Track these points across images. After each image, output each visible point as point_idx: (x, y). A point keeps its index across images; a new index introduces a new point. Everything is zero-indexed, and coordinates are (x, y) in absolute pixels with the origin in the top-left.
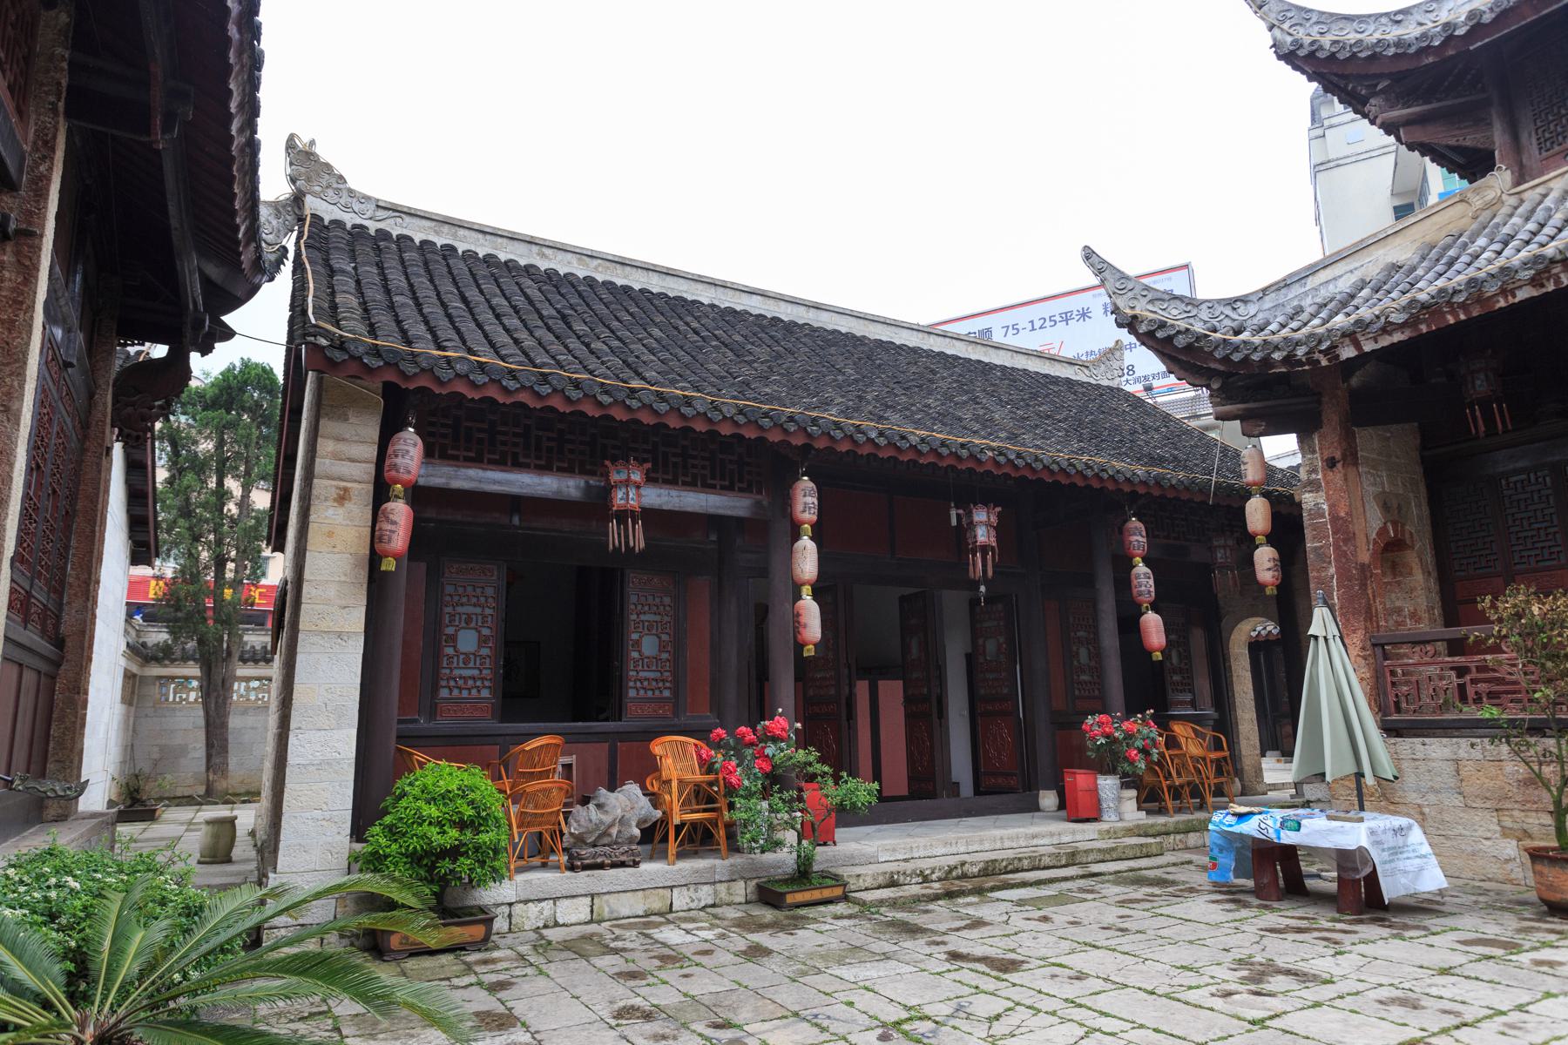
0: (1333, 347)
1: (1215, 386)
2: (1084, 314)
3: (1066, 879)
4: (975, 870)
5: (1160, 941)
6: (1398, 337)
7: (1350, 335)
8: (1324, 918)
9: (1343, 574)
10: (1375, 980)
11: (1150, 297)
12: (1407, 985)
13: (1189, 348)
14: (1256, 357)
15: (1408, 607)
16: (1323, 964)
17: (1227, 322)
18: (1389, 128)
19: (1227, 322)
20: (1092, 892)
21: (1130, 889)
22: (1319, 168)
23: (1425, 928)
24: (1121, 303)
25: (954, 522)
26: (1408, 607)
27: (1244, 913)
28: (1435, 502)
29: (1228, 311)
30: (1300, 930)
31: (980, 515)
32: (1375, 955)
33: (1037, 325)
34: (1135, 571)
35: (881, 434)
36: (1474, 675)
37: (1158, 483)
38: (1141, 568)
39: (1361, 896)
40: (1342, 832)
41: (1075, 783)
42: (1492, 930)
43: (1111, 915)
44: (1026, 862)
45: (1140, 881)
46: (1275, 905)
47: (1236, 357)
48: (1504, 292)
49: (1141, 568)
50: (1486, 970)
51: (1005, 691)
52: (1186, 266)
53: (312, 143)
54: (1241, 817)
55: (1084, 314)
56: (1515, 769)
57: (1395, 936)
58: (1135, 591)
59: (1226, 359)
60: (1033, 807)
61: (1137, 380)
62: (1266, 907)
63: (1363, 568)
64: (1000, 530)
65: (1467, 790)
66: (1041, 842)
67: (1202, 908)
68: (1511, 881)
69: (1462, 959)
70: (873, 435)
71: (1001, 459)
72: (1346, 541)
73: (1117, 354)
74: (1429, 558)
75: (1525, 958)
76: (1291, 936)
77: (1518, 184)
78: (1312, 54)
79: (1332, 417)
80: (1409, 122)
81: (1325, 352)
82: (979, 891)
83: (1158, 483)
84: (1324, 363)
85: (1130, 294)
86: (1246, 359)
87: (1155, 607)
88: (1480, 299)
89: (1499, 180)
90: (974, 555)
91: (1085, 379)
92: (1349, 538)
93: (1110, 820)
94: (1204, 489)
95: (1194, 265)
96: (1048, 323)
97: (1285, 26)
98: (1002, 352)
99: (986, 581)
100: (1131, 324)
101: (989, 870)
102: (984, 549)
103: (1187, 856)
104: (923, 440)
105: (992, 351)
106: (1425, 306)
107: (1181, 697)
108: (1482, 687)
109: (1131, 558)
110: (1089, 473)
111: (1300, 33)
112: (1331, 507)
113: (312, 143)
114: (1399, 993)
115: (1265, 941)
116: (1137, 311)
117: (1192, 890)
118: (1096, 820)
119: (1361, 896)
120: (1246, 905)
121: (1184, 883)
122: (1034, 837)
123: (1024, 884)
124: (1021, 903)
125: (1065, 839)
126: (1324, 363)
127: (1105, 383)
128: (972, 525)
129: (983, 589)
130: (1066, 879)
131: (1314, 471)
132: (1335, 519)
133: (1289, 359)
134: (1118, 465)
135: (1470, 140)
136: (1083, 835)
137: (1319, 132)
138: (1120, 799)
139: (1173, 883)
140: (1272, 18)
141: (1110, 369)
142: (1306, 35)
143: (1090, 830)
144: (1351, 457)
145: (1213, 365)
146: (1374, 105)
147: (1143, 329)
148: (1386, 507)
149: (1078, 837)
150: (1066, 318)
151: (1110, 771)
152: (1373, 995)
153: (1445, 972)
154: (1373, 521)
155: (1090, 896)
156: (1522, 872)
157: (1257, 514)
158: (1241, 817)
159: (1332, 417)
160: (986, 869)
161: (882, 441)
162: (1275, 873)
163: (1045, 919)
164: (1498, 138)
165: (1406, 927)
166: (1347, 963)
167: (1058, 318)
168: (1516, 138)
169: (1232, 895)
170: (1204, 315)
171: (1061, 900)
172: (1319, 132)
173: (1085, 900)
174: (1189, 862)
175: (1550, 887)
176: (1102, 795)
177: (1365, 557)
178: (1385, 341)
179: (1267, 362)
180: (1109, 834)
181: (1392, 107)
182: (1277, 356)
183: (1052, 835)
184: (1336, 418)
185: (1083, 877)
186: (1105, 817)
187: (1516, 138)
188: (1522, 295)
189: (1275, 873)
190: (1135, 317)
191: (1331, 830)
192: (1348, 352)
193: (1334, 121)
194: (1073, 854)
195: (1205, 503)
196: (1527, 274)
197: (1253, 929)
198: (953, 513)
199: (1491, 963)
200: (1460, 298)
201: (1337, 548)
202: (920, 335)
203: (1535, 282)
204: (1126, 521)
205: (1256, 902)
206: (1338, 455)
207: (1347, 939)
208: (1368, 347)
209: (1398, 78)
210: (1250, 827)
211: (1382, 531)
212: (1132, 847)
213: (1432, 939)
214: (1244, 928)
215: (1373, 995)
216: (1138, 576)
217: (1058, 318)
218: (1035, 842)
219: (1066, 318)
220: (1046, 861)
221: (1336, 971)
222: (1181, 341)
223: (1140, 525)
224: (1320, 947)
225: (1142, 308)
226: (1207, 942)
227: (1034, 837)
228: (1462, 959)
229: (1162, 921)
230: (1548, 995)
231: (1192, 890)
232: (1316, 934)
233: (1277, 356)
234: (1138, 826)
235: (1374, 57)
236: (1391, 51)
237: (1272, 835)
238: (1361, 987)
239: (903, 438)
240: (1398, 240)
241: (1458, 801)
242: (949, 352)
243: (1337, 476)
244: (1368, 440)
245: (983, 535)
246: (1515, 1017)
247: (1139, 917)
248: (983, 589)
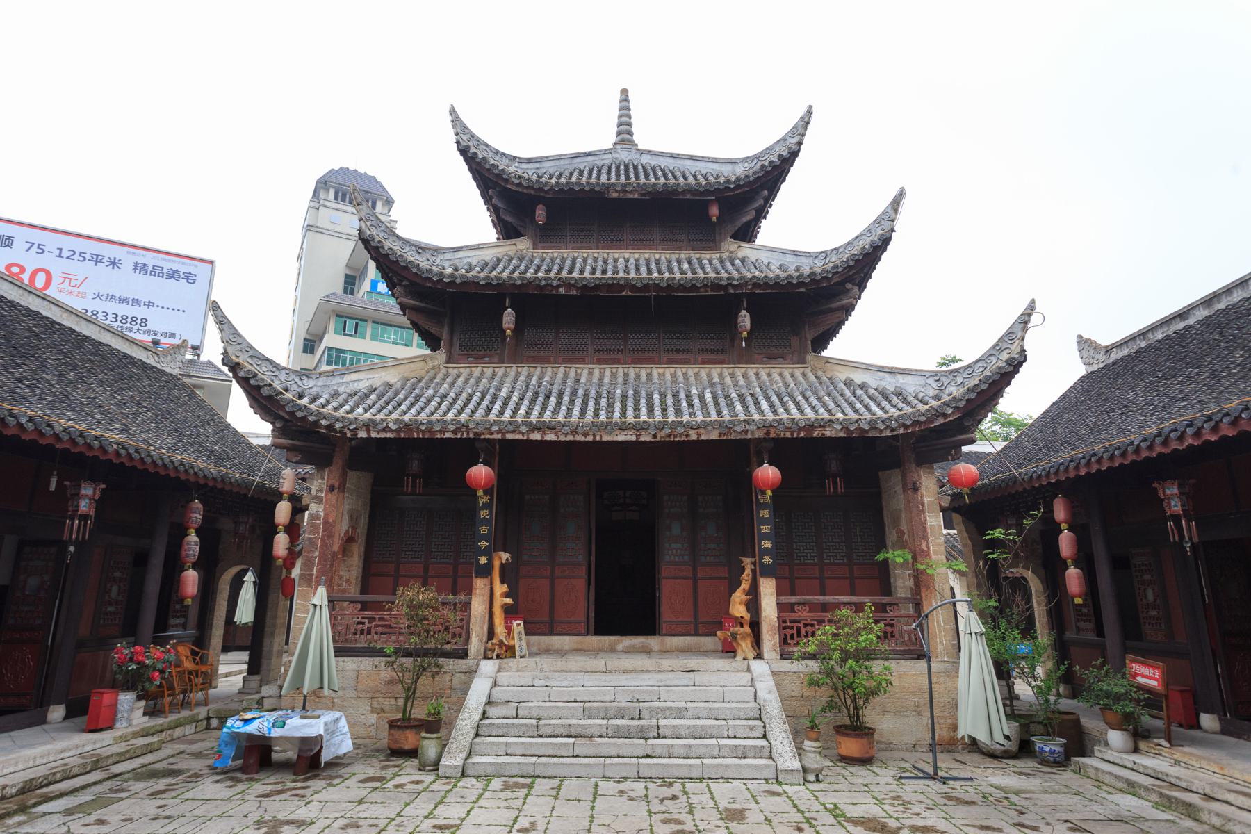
0: (356, 429)
1: (278, 425)
2: (114, 263)
3: (95, 784)
4: (14, 790)
5: (200, 820)
6: (389, 435)
7: (367, 426)
8: (288, 780)
9: (323, 556)
10: (333, 815)
11: (251, 353)
12: (348, 815)
13: (270, 398)
14: (311, 419)
15: (346, 575)
16: (302, 813)
17: (295, 387)
18: (403, 307)
19: (295, 387)
20: (122, 790)
21: (151, 783)
22: (310, 228)
23: (341, 777)
24: (230, 350)
25: (53, 487)
26: (346, 575)
27: (240, 787)
28: (372, 517)
29: (297, 380)
30: (279, 792)
31: (87, 490)
32: (324, 803)
33: (65, 253)
34: (188, 538)
35: (30, 420)
36: (377, 622)
37: (223, 480)
38: (193, 538)
39: (309, 762)
40: (310, 726)
41: (101, 701)
42: (371, 772)
43: (151, 807)
44: (58, 775)
45: (154, 775)
46: (256, 776)
47: (299, 414)
48: (441, 431)
49: (193, 538)
50: (376, 796)
51: (39, 622)
52: (211, 262)
53: (1085, 344)
54: (246, 721)
55: (114, 263)
56: (386, 674)
57: (330, 785)
58: (183, 553)
59: (292, 413)
60: (42, 720)
61: (147, 332)
62: (251, 779)
63: (334, 554)
64: (100, 504)
65: (360, 687)
66: (67, 755)
67: (210, 788)
68: (369, 737)
69: (364, 793)
70: (24, 420)
71: (123, 452)
72: (329, 537)
73: (182, 350)
74: (362, 549)
75: (390, 785)
76: (277, 798)
77: (448, 362)
78: (377, 248)
79: (338, 462)
80: (413, 308)
81: (351, 431)
82: (23, 809)
83: (223, 480)
84: (349, 435)
85: (238, 347)
86: (304, 418)
87: (195, 566)
88: (430, 430)
89: (441, 356)
90: (72, 520)
91: (154, 364)
92: (331, 536)
93: (121, 728)
94: (248, 485)
95: (217, 264)
96: (76, 257)
97: (369, 223)
98: (92, 326)
99: (77, 544)
100: (234, 367)
101: (28, 788)
102: (84, 517)
103: (182, 747)
104: (65, 430)
105: (84, 323)
106: (406, 425)
107: (178, 621)
108: (379, 629)
109: (187, 528)
110: (182, 468)
111: (374, 232)
112: (326, 515)
113: (1085, 344)
114: (347, 821)
115: (264, 804)
116: (240, 360)
117: (196, 775)
118: (111, 728)
119: (309, 762)
120: (239, 781)
121: (188, 770)
122: (63, 751)
123: (62, 795)
124: (69, 812)
125: (87, 749)
126: (349, 435)
127: (168, 370)
128: (77, 496)
129: (72, 549)
130: (95, 784)
131: (321, 491)
132: (326, 522)
133: (330, 427)
134: (202, 465)
135: (434, 330)
136: (101, 742)
137: (316, 205)
138: (132, 709)
139: (180, 772)
140: (363, 215)
141: (175, 360)
142: (378, 235)
143: (105, 737)
144: (342, 488)
145: (282, 413)
146: (398, 290)
147: (241, 374)
148: (351, 518)
149: (98, 745)
150: (97, 259)
151: (128, 688)
152: (336, 825)
153: (360, 802)
154: (343, 526)
155: (124, 795)
156: (384, 733)
157: (283, 511)
158: (246, 721)
159: (338, 462)
160: (23, 788)
161: (30, 426)
162: (257, 757)
163: (100, 822)
164: (445, 335)
165: (332, 778)
166: (315, 806)
167: (88, 257)
168: (451, 339)
169: (226, 775)
170: (283, 377)
171: (100, 802)
172: (316, 205)
173: (121, 799)
174: (182, 752)
175: (396, 742)
176: (120, 708)
177: (336, 548)
178: (383, 435)
179: (317, 423)
180: (124, 739)
181: (406, 296)
182: (324, 422)
183: (77, 747)
184: (341, 463)
185: (108, 779)
186: (118, 725)
187: (451, 339)
188: (448, 435)
189: (257, 757)
190: (238, 364)
191: (303, 726)
192: (362, 434)
193: (327, 203)
194: (97, 761)
195: (245, 495)
196: (452, 427)
197: (252, 797)
198: (54, 480)
199: (377, 792)
200: (423, 427)
201: (323, 540)
202: (21, 291)
203: (454, 432)
204: (192, 500)
205: (244, 777)
206: (337, 485)
207: (307, 792)
208: (374, 435)
209: (412, 283)
210: (252, 728)
211: (347, 531)
212: (141, 747)
213: (347, 783)
214: (247, 798)
215: (336, 825)
216: (189, 543)
217: (88, 257)
218: (62, 756)
219: (97, 259)
220: (76, 771)
221: (312, 815)
222: (265, 392)
223: (200, 506)
224: (296, 802)
225: (243, 359)
226: (230, 813)
227: (63, 751)
228: (364, 793)
229: (189, 805)
230: (407, 804)
231: (196, 775)
232: (290, 793)
233: (324, 422)
234: (143, 729)
235: (406, 268)
236: (415, 270)
237: (266, 732)
238: (328, 822)
239: (49, 425)
240: (392, 370)
241: (353, 694)
242: (45, 313)
243: (333, 497)
244: (352, 476)
245: (84, 506)
246: (398, 820)
247: (173, 806)
248: (72, 549)
